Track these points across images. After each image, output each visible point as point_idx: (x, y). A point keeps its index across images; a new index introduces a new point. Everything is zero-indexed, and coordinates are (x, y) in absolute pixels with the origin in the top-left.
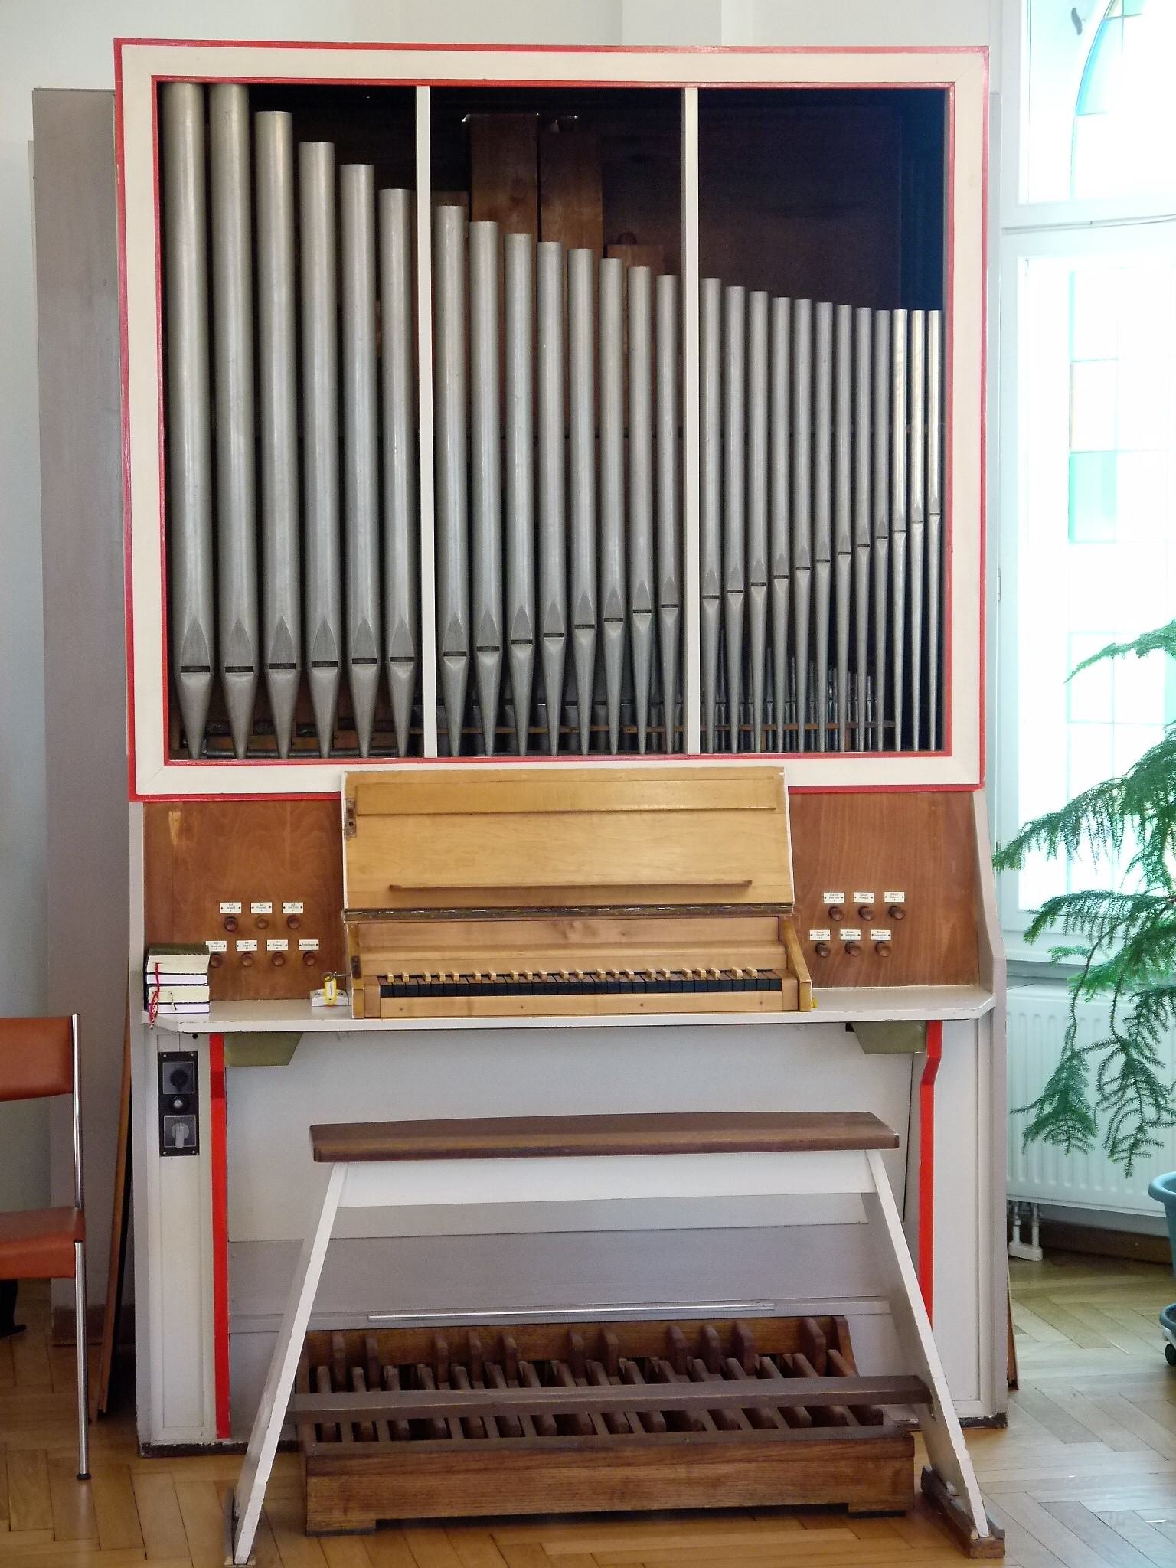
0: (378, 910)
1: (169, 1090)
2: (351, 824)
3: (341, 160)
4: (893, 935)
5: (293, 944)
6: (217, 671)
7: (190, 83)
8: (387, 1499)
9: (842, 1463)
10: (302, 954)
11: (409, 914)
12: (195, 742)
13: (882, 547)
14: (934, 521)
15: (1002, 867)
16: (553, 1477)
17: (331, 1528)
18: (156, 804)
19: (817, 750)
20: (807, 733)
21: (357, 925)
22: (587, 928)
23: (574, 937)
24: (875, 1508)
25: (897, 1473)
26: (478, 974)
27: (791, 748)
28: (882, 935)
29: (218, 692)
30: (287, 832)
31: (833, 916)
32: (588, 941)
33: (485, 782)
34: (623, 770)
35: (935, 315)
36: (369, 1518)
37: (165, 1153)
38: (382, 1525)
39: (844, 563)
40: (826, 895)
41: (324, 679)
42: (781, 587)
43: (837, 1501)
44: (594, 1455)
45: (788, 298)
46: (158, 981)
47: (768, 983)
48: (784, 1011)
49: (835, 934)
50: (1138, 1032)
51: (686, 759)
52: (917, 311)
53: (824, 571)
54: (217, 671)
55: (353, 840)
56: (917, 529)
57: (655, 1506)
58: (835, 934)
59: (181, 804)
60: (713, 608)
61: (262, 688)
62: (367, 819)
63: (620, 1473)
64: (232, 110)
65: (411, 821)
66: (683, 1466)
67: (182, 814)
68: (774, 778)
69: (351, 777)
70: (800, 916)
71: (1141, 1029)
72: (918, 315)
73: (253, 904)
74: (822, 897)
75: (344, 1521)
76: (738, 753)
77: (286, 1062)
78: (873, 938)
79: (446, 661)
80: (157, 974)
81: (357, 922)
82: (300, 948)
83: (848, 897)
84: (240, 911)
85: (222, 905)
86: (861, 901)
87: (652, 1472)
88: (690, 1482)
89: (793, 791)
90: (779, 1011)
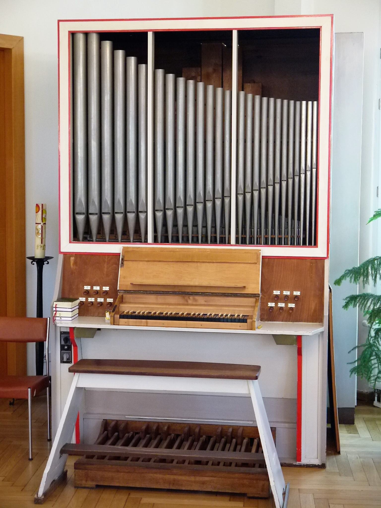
0: (128, 290)
1: (63, 343)
2: (122, 263)
3: (127, 55)
4: (296, 305)
5: (105, 300)
6: (87, 214)
7: (81, 33)
8: (99, 479)
9: (245, 480)
10: (289, 308)
11: (138, 292)
12: (81, 236)
13: (297, 179)
14: (314, 170)
15: (336, 285)
16: (151, 477)
17: (81, 486)
18: (67, 255)
19: (275, 244)
20: (272, 238)
21: (122, 295)
22: (194, 299)
23: (190, 302)
24: (256, 496)
25: (263, 485)
26: (236, 315)
27: (266, 243)
28: (292, 305)
29: (87, 221)
30: (106, 265)
31: (277, 299)
32: (194, 303)
33: (165, 251)
34: (209, 249)
35: (315, 103)
36: (93, 484)
37: (62, 362)
38: (98, 486)
39: (284, 184)
40: (274, 291)
41: (119, 217)
42: (263, 191)
43: (243, 492)
44: (164, 471)
45: (287, 100)
46: (56, 310)
47: (243, 320)
48: (247, 330)
49: (276, 304)
50: (375, 342)
51: (230, 246)
52: (310, 102)
53: (277, 186)
54: (87, 214)
55: (122, 268)
56: (309, 173)
57: (184, 489)
58: (276, 304)
59: (75, 255)
60: (241, 198)
61: (113, 220)
62: (126, 261)
63: (172, 477)
64: (94, 41)
65: (141, 263)
66: (193, 477)
67: (74, 259)
68: (257, 253)
69: (124, 248)
70: (265, 298)
71: (376, 341)
72: (310, 103)
73: (94, 287)
74: (273, 292)
75: (85, 484)
76: (228, 244)
77: (93, 337)
78: (289, 306)
79: (156, 212)
80: (56, 307)
81: (123, 294)
82: (107, 301)
83: (282, 292)
84: (90, 289)
85: (85, 287)
86: (296, 294)
87: (180, 478)
88: (195, 482)
89: (263, 257)
90: (145, 326)
